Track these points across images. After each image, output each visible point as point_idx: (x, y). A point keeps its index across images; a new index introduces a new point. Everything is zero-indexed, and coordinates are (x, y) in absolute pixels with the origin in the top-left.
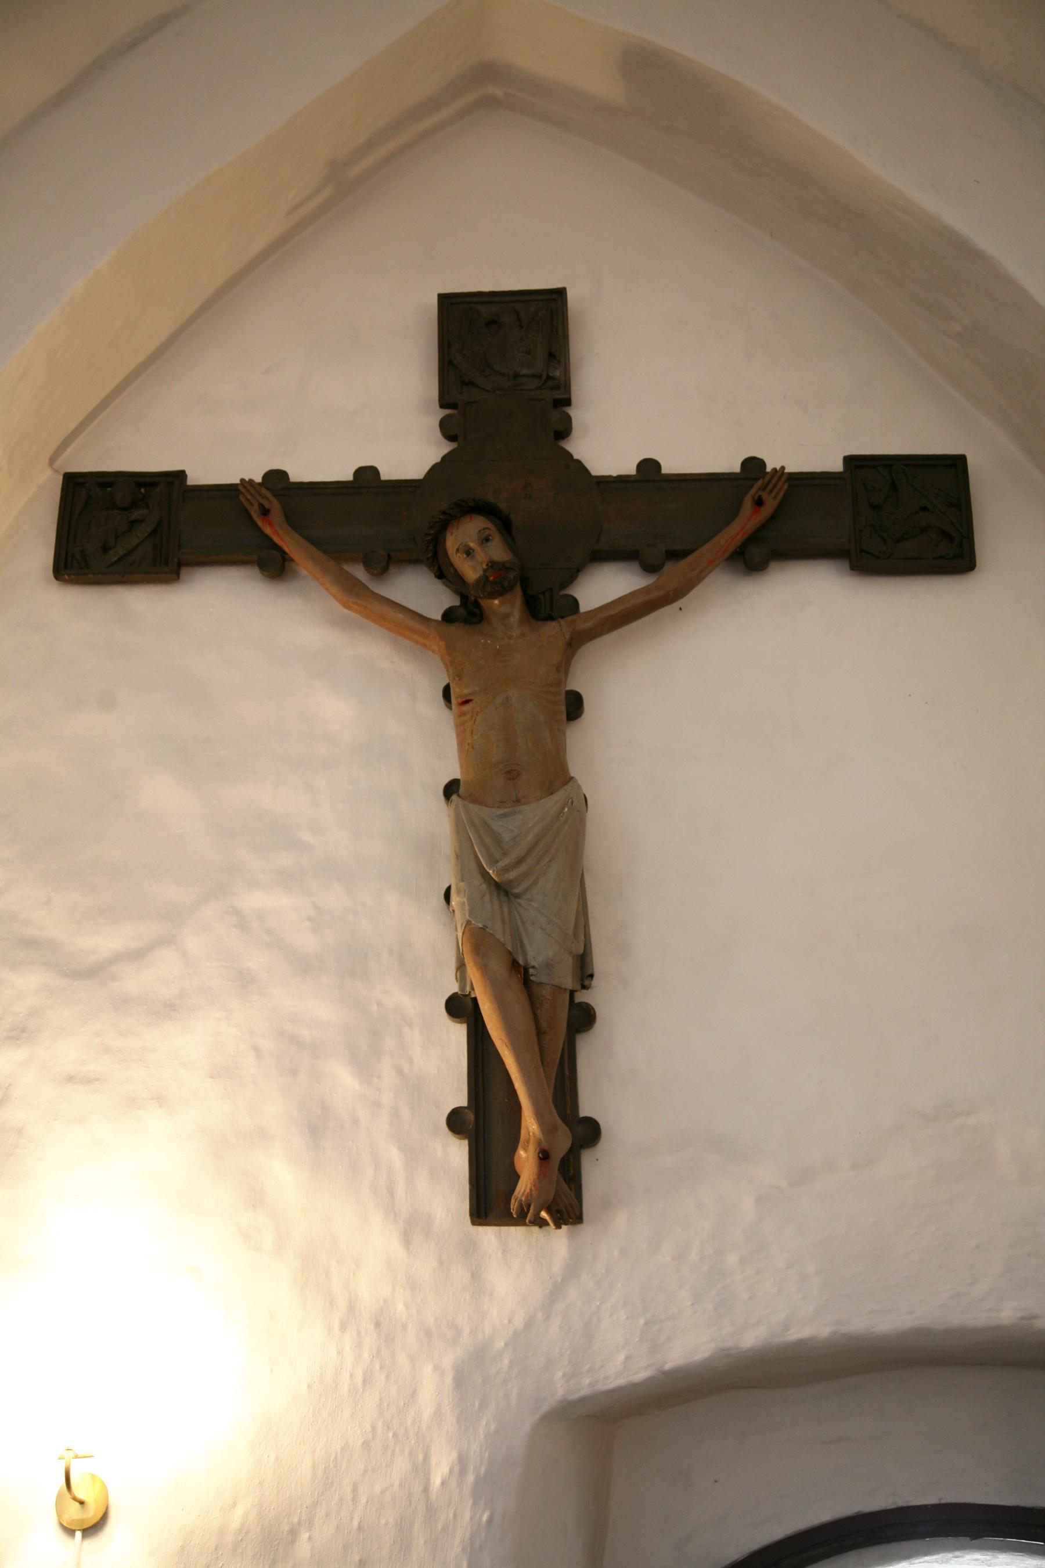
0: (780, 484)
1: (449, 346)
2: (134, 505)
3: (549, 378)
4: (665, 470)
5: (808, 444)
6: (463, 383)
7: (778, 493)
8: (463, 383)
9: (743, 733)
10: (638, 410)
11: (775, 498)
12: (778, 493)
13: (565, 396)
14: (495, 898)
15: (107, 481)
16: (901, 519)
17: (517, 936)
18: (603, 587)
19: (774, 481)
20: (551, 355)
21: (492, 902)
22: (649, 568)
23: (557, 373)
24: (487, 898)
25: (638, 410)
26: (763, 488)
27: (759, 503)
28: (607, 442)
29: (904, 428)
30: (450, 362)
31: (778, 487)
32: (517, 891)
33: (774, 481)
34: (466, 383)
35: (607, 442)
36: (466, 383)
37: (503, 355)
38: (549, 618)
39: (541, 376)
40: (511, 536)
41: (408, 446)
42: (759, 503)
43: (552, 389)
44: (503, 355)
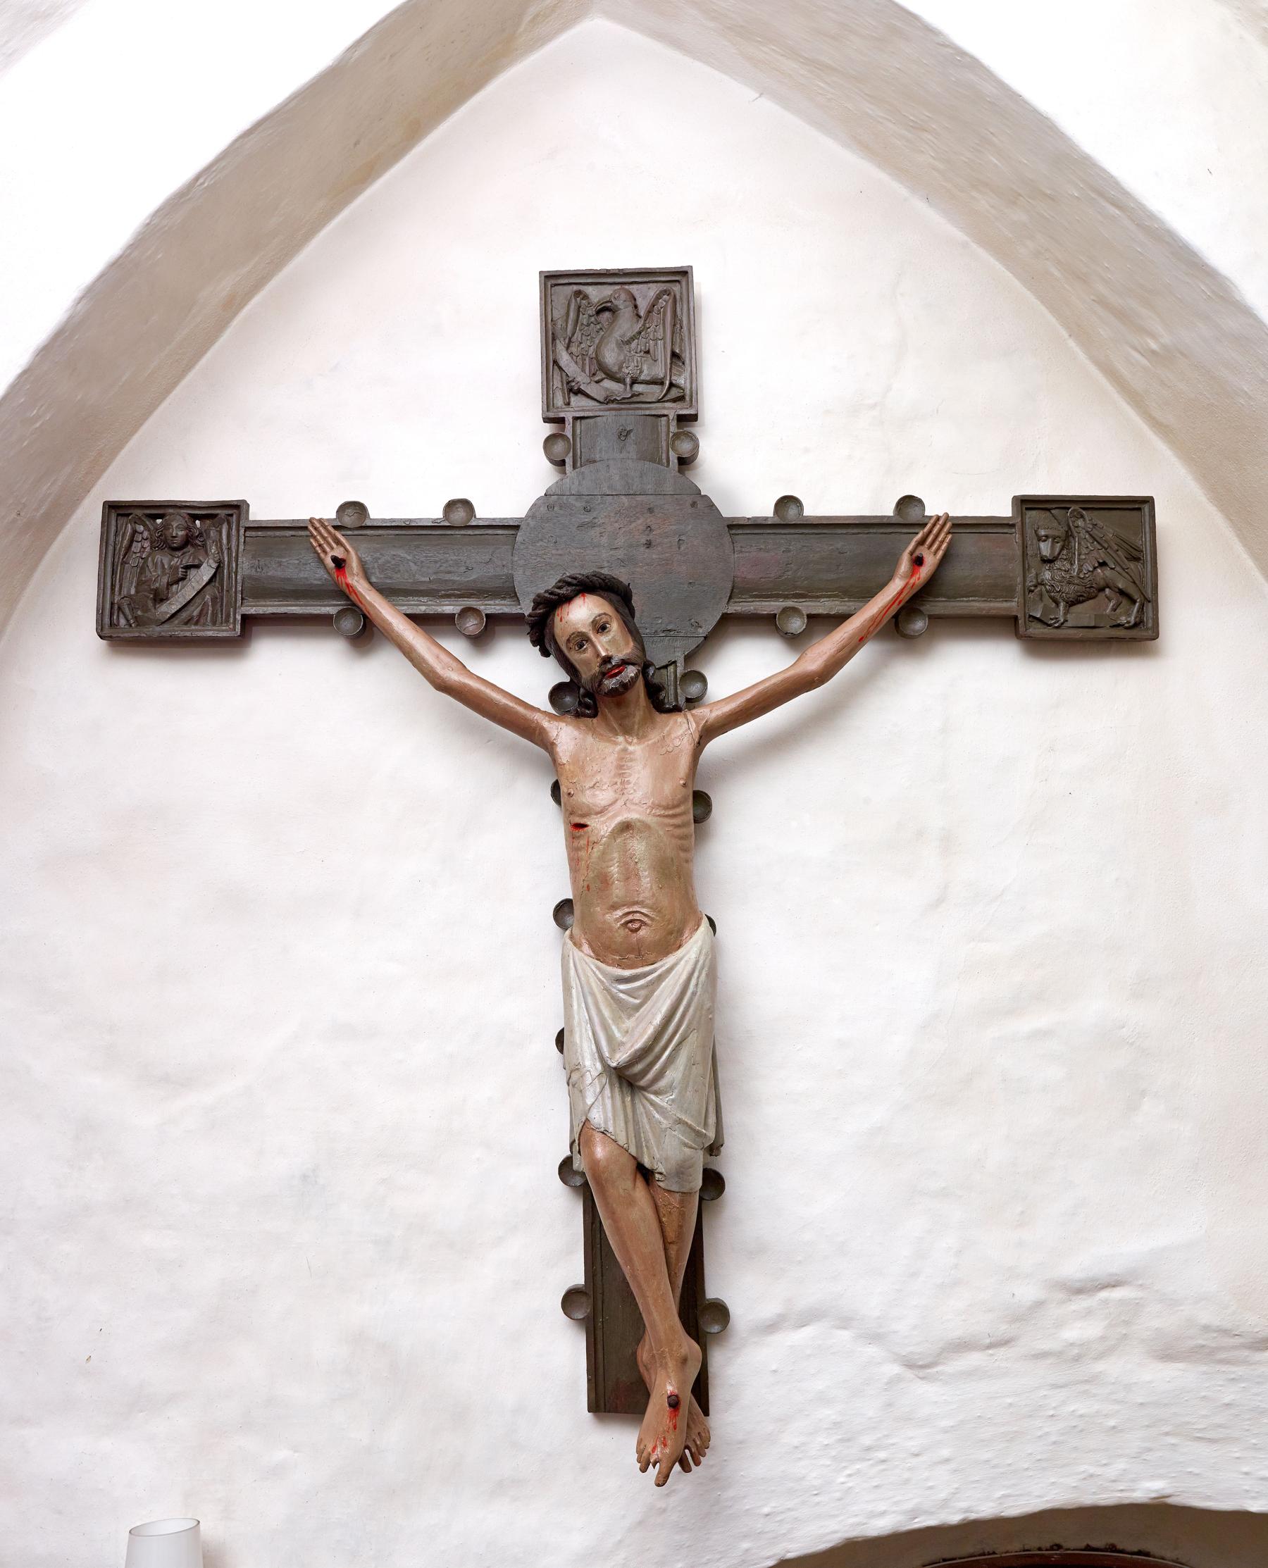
0: (942, 535)
1: (554, 340)
2: (188, 541)
3: (672, 385)
4: (579, 1279)
5: (971, 485)
6: (571, 390)
7: (938, 548)
8: (571, 390)
9: (896, 846)
10: (776, 439)
11: (935, 553)
12: (938, 548)
13: (692, 412)
14: (617, 1090)
15: (156, 511)
16: (1074, 580)
17: (639, 1146)
18: (741, 667)
19: (935, 531)
20: (674, 355)
21: (612, 1097)
22: (794, 641)
23: (681, 381)
24: (607, 1091)
25: (776, 439)
26: (921, 542)
27: (918, 562)
28: (745, 466)
29: (1086, 462)
30: (555, 362)
31: (940, 539)
32: (642, 1083)
33: (935, 531)
34: (574, 390)
35: (745, 466)
36: (574, 390)
37: (618, 346)
38: (677, 709)
39: (662, 383)
40: (635, 600)
41: (507, 473)
42: (918, 562)
43: (674, 400)
44: (618, 346)
